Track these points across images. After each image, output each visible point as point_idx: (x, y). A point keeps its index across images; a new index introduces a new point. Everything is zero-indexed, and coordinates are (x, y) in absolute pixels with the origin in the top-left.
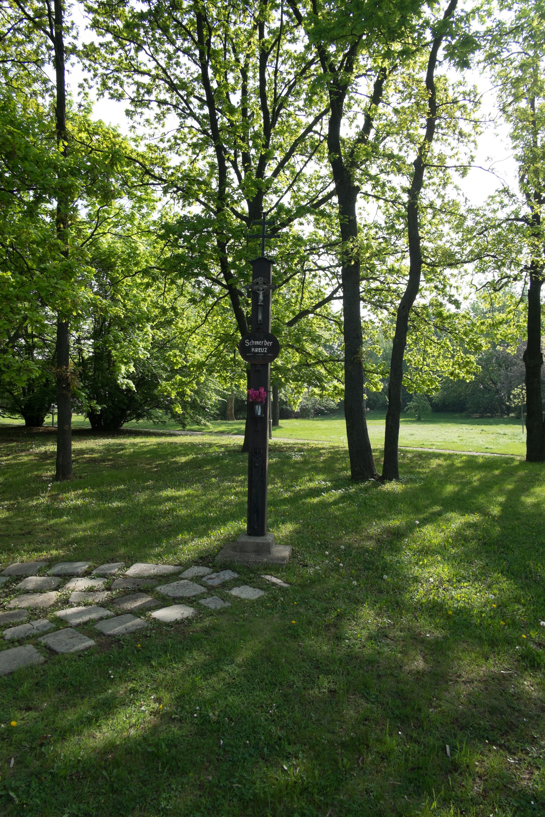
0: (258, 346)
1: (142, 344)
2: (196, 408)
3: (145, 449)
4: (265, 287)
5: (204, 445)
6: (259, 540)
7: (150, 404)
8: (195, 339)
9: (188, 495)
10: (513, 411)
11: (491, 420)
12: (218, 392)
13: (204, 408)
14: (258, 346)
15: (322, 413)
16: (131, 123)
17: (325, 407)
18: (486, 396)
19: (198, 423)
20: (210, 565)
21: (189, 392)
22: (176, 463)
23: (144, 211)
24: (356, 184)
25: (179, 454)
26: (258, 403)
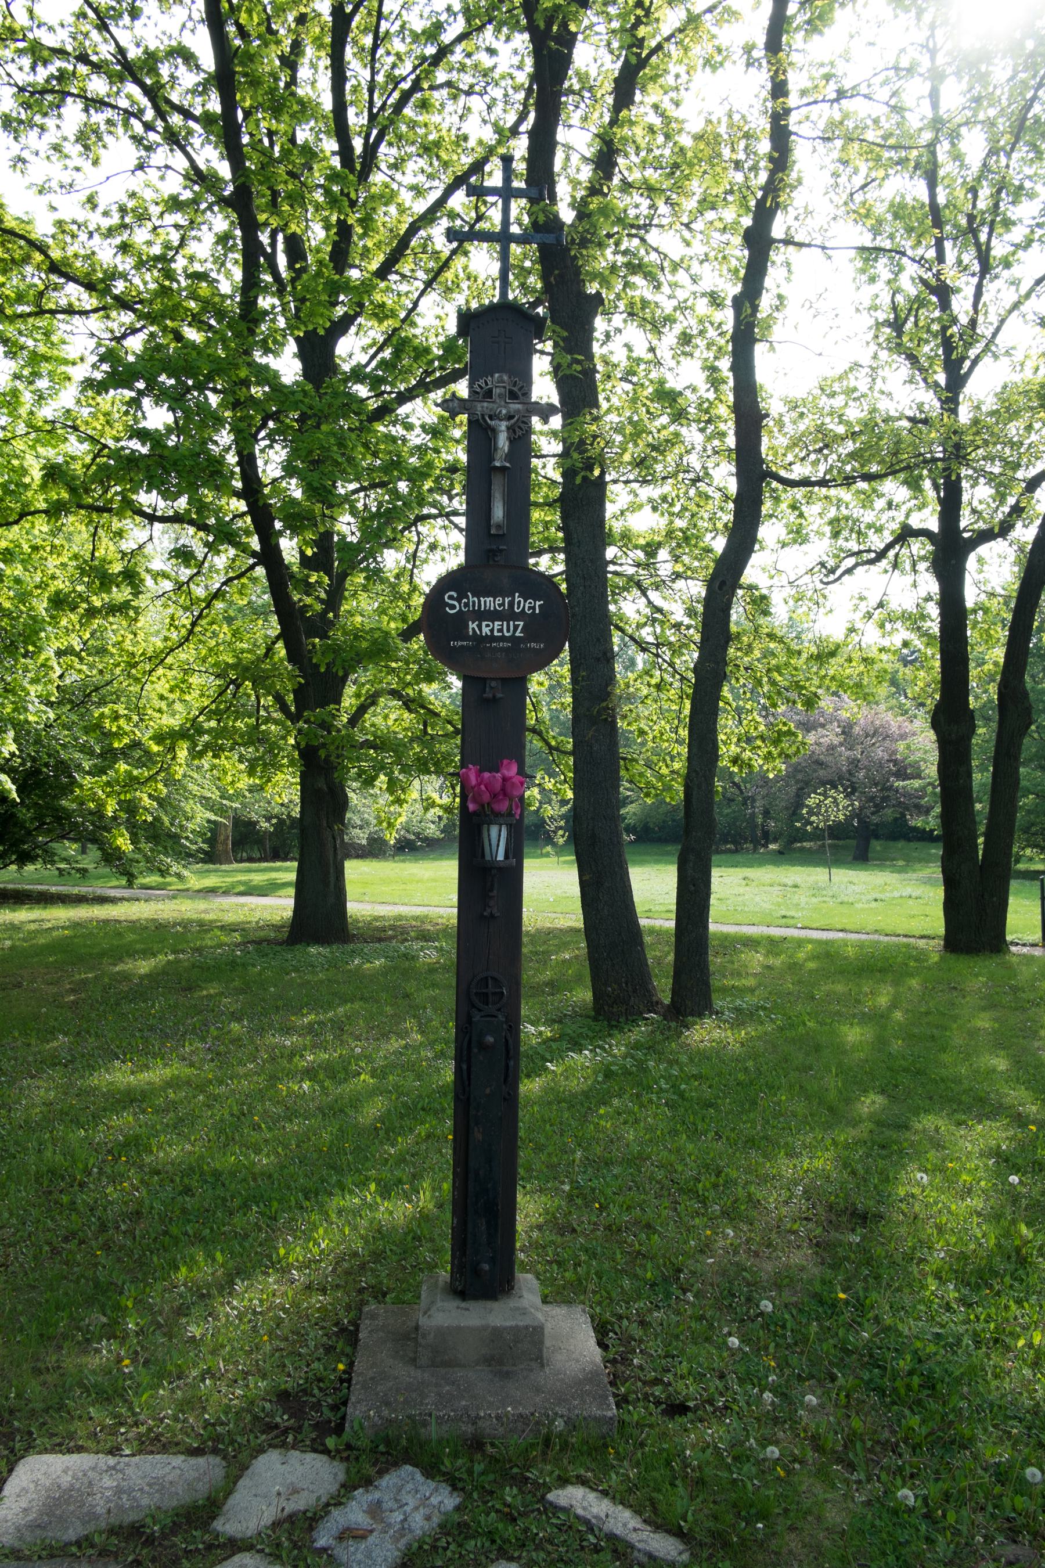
0: (493, 616)
1: (33, 690)
2: (160, 838)
3: (42, 941)
4: (515, 406)
5: (186, 924)
6: (495, 1315)
7: (49, 831)
8: (161, 683)
9: (172, 1083)
10: (775, 840)
11: (738, 857)
12: (206, 802)
13: (176, 837)
14: (493, 616)
15: (411, 846)
16: (15, 149)
17: (417, 835)
18: (726, 811)
19: (163, 873)
20: (331, 1442)
21: (146, 801)
22: (126, 977)
23: (43, 384)
24: (592, 288)
25: (132, 953)
26: (496, 817)
